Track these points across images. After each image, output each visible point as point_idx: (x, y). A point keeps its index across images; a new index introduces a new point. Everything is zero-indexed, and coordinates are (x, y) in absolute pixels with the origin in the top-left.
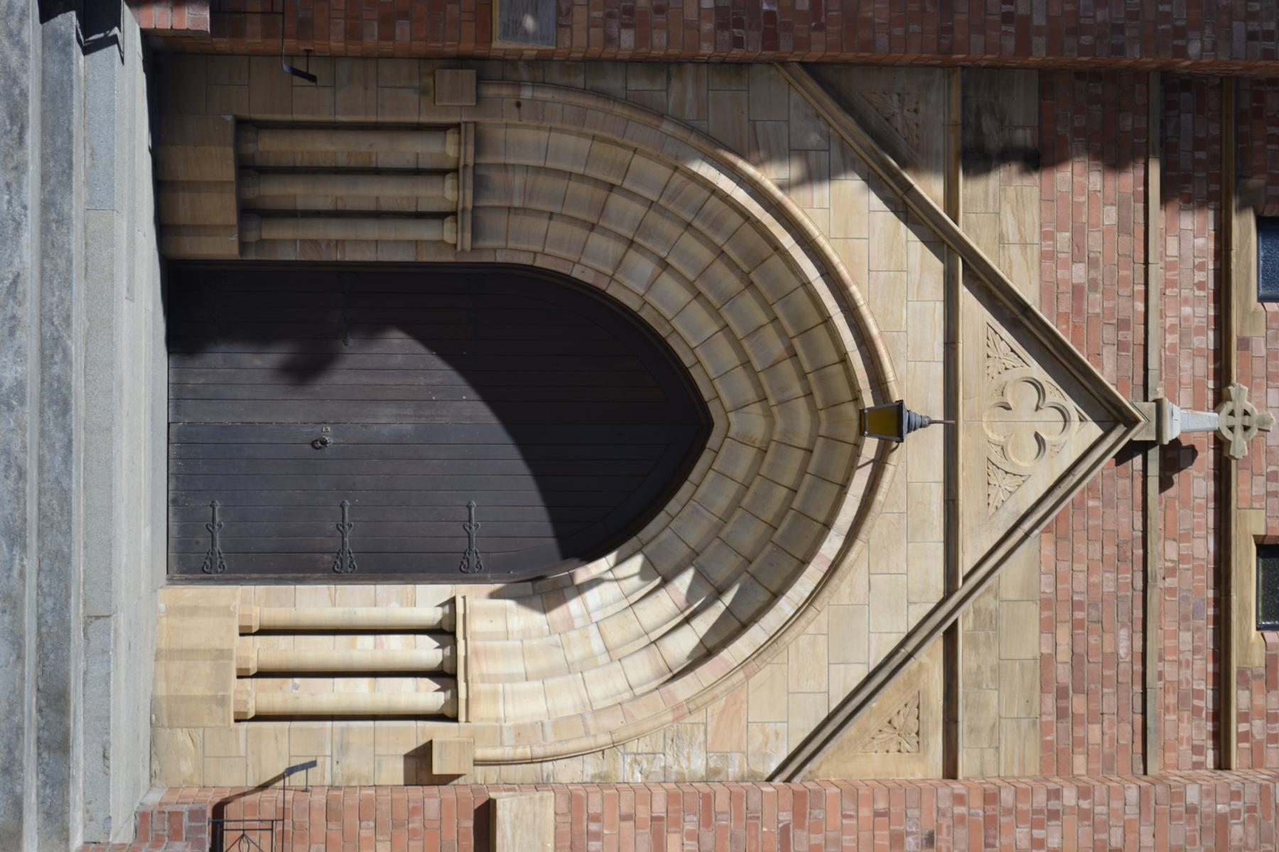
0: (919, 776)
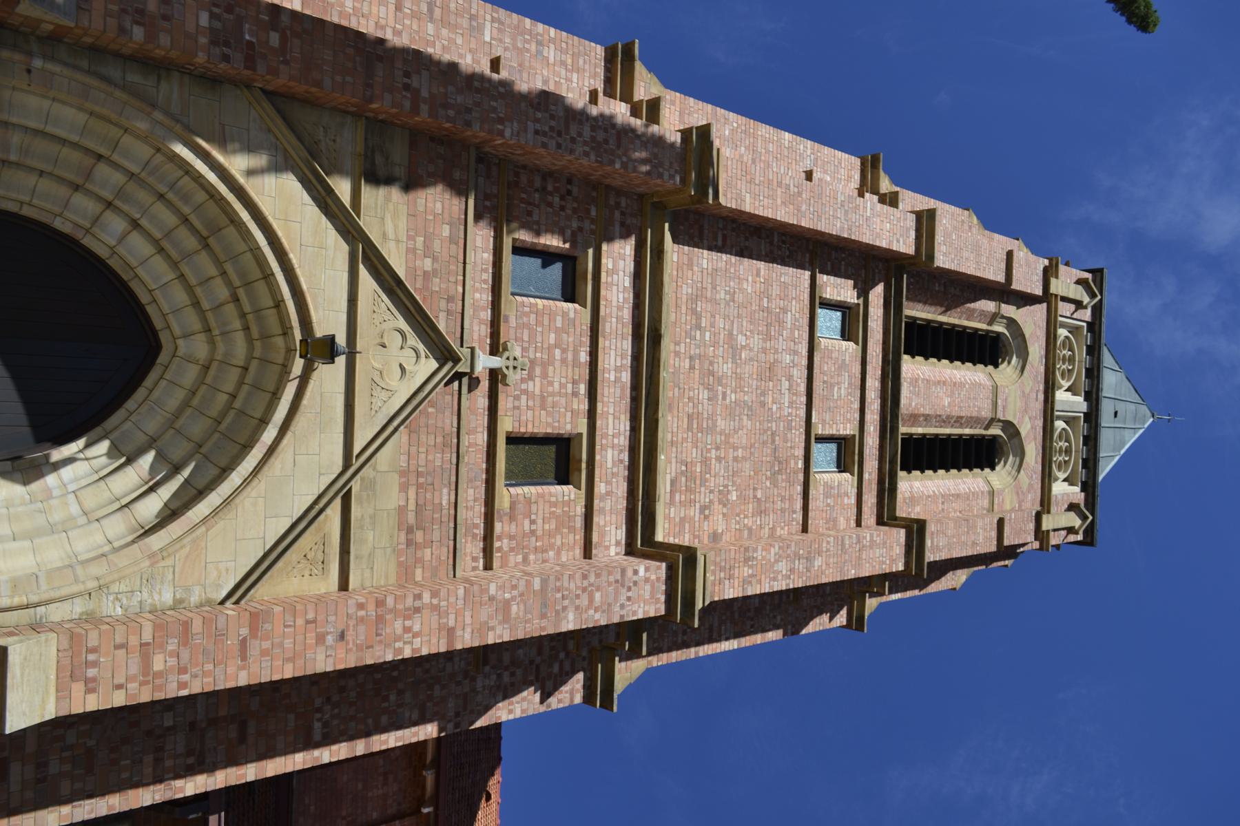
0: (323, 591)
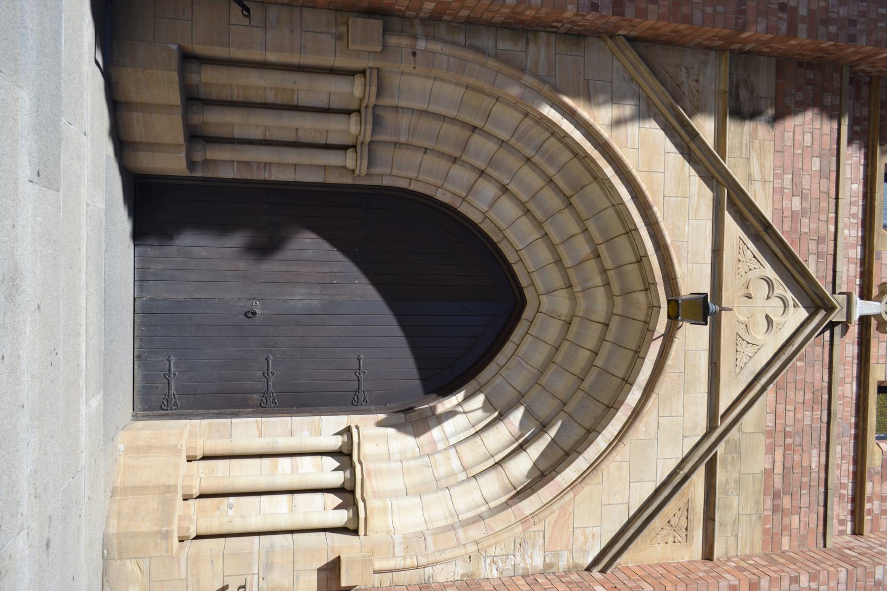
0: (687, 559)
